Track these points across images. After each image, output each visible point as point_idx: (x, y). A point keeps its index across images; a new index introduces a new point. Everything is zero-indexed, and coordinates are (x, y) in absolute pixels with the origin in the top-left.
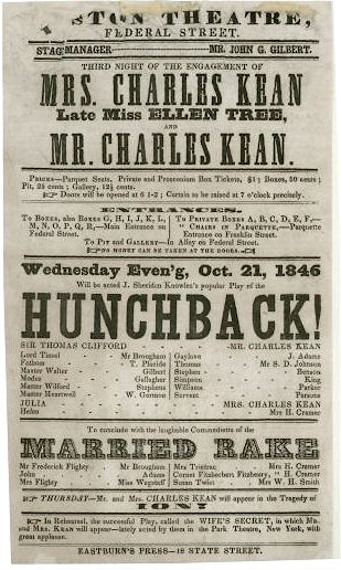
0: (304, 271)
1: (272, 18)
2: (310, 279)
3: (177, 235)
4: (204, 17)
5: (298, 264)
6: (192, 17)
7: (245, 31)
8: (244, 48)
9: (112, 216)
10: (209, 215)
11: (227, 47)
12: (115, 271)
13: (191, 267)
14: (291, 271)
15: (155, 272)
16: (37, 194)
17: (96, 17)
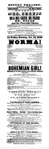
0: (40, 37)
1: (37, 5)
2: (41, 38)
3: (25, 33)
4: (29, 5)
5: (40, 36)
6: (27, 5)
7: (33, 6)
8: (33, 9)
9: (18, 31)
10: (29, 31)
11: (31, 8)
12: (17, 37)
13: (28, 37)
14: (39, 37)
15: (22, 37)
16: (34, 30)
17: (16, 5)
